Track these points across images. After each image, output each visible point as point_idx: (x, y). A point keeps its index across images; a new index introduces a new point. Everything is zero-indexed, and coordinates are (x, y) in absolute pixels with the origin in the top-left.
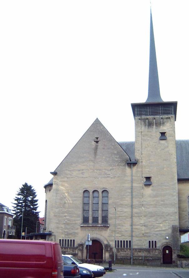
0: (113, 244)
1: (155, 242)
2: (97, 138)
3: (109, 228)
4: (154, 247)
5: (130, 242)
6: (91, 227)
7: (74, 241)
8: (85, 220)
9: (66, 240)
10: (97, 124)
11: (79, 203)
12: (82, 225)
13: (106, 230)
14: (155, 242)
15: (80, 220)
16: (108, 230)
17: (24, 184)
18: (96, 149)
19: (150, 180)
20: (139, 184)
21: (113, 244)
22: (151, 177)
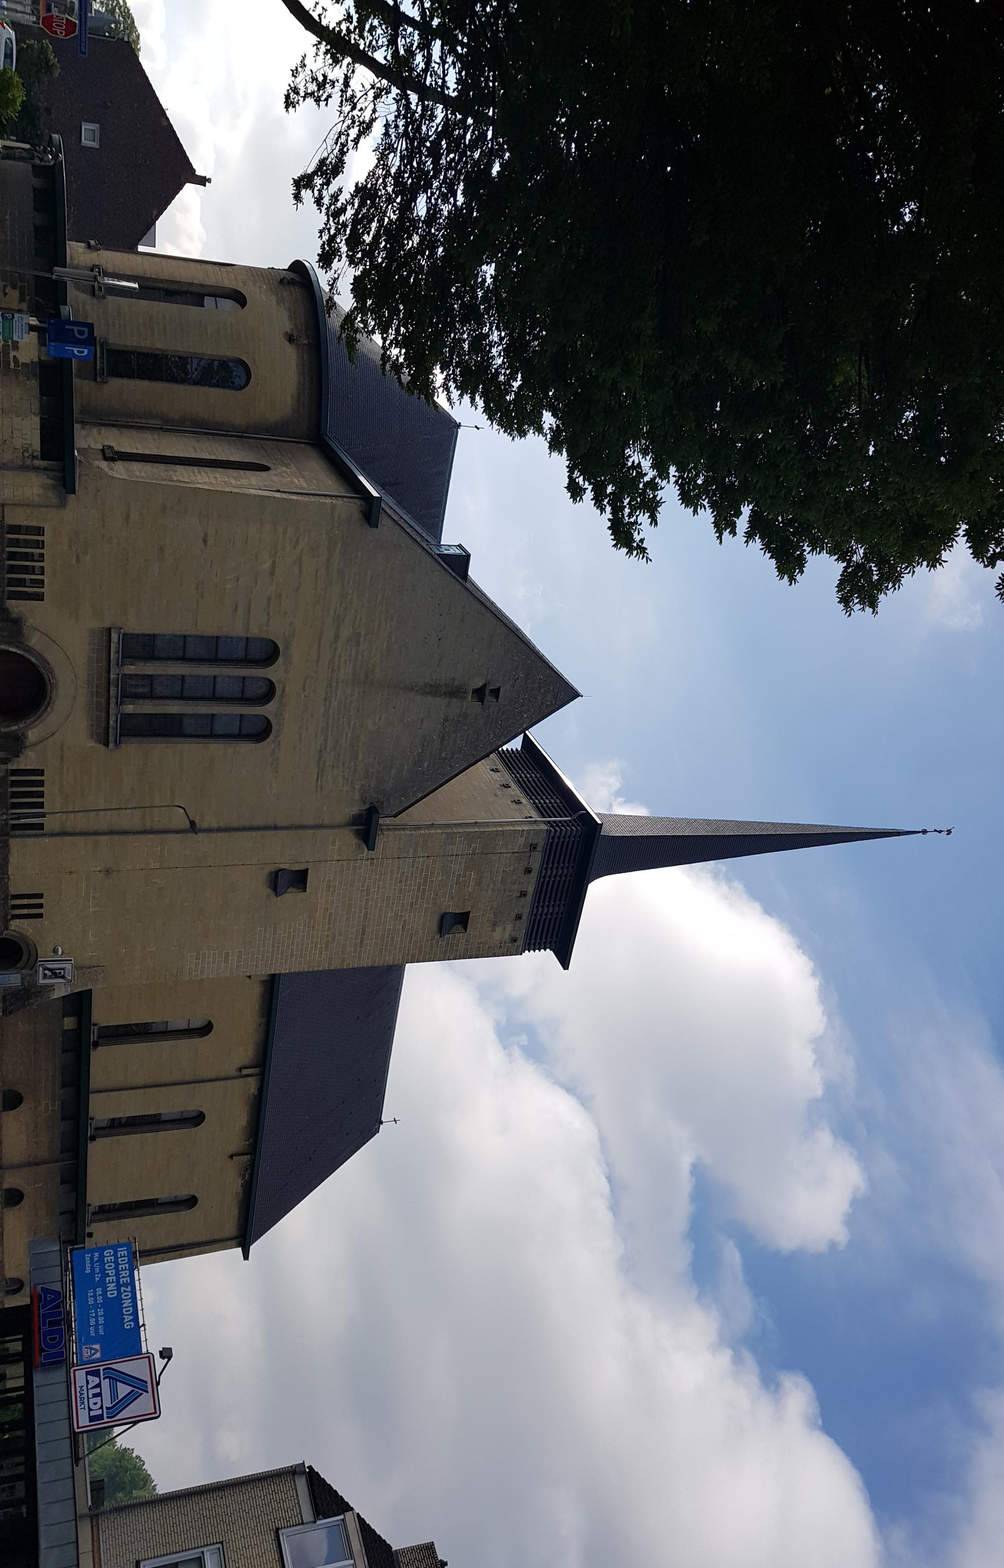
0: (27, 760)
1: (40, 916)
2: (496, 692)
3: (101, 746)
4: (14, 778)
5: (41, 826)
6: (104, 674)
7: (40, 597)
8: (142, 647)
9: (40, 545)
10: (573, 694)
11: (213, 621)
12: (114, 636)
13: (92, 735)
14: (40, 916)
15: (136, 624)
16: (91, 743)
17: (861, 614)
18: (454, 692)
19: (292, 885)
20: (284, 852)
21: (27, 760)
22: (304, 889)
